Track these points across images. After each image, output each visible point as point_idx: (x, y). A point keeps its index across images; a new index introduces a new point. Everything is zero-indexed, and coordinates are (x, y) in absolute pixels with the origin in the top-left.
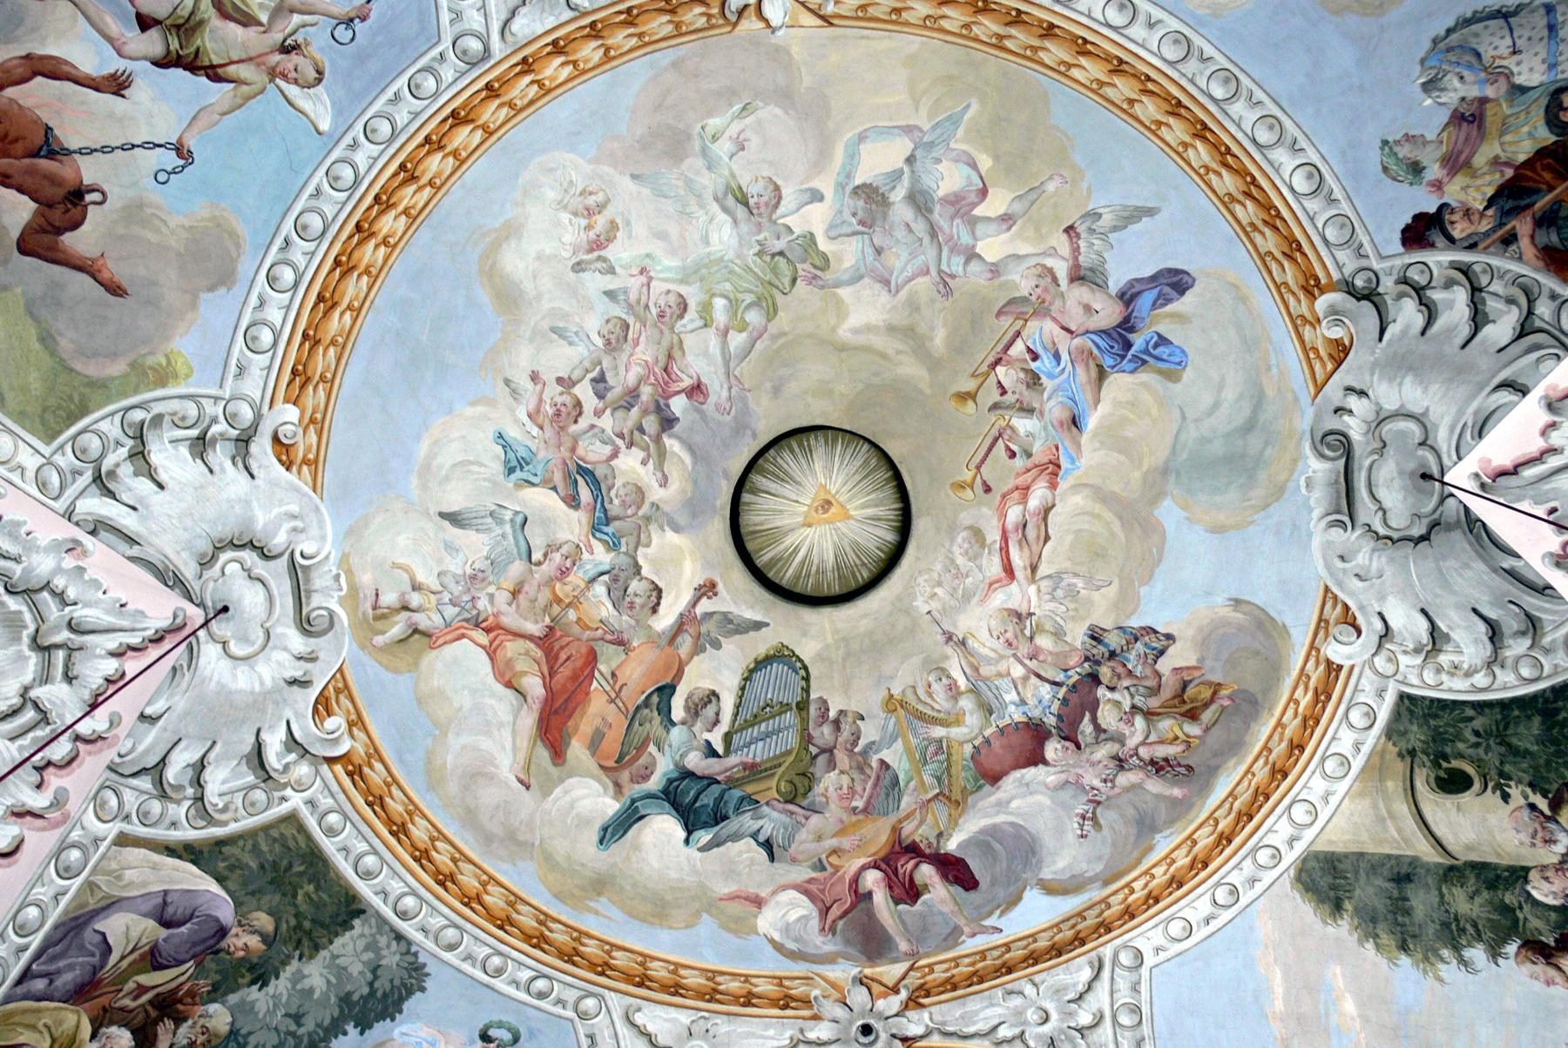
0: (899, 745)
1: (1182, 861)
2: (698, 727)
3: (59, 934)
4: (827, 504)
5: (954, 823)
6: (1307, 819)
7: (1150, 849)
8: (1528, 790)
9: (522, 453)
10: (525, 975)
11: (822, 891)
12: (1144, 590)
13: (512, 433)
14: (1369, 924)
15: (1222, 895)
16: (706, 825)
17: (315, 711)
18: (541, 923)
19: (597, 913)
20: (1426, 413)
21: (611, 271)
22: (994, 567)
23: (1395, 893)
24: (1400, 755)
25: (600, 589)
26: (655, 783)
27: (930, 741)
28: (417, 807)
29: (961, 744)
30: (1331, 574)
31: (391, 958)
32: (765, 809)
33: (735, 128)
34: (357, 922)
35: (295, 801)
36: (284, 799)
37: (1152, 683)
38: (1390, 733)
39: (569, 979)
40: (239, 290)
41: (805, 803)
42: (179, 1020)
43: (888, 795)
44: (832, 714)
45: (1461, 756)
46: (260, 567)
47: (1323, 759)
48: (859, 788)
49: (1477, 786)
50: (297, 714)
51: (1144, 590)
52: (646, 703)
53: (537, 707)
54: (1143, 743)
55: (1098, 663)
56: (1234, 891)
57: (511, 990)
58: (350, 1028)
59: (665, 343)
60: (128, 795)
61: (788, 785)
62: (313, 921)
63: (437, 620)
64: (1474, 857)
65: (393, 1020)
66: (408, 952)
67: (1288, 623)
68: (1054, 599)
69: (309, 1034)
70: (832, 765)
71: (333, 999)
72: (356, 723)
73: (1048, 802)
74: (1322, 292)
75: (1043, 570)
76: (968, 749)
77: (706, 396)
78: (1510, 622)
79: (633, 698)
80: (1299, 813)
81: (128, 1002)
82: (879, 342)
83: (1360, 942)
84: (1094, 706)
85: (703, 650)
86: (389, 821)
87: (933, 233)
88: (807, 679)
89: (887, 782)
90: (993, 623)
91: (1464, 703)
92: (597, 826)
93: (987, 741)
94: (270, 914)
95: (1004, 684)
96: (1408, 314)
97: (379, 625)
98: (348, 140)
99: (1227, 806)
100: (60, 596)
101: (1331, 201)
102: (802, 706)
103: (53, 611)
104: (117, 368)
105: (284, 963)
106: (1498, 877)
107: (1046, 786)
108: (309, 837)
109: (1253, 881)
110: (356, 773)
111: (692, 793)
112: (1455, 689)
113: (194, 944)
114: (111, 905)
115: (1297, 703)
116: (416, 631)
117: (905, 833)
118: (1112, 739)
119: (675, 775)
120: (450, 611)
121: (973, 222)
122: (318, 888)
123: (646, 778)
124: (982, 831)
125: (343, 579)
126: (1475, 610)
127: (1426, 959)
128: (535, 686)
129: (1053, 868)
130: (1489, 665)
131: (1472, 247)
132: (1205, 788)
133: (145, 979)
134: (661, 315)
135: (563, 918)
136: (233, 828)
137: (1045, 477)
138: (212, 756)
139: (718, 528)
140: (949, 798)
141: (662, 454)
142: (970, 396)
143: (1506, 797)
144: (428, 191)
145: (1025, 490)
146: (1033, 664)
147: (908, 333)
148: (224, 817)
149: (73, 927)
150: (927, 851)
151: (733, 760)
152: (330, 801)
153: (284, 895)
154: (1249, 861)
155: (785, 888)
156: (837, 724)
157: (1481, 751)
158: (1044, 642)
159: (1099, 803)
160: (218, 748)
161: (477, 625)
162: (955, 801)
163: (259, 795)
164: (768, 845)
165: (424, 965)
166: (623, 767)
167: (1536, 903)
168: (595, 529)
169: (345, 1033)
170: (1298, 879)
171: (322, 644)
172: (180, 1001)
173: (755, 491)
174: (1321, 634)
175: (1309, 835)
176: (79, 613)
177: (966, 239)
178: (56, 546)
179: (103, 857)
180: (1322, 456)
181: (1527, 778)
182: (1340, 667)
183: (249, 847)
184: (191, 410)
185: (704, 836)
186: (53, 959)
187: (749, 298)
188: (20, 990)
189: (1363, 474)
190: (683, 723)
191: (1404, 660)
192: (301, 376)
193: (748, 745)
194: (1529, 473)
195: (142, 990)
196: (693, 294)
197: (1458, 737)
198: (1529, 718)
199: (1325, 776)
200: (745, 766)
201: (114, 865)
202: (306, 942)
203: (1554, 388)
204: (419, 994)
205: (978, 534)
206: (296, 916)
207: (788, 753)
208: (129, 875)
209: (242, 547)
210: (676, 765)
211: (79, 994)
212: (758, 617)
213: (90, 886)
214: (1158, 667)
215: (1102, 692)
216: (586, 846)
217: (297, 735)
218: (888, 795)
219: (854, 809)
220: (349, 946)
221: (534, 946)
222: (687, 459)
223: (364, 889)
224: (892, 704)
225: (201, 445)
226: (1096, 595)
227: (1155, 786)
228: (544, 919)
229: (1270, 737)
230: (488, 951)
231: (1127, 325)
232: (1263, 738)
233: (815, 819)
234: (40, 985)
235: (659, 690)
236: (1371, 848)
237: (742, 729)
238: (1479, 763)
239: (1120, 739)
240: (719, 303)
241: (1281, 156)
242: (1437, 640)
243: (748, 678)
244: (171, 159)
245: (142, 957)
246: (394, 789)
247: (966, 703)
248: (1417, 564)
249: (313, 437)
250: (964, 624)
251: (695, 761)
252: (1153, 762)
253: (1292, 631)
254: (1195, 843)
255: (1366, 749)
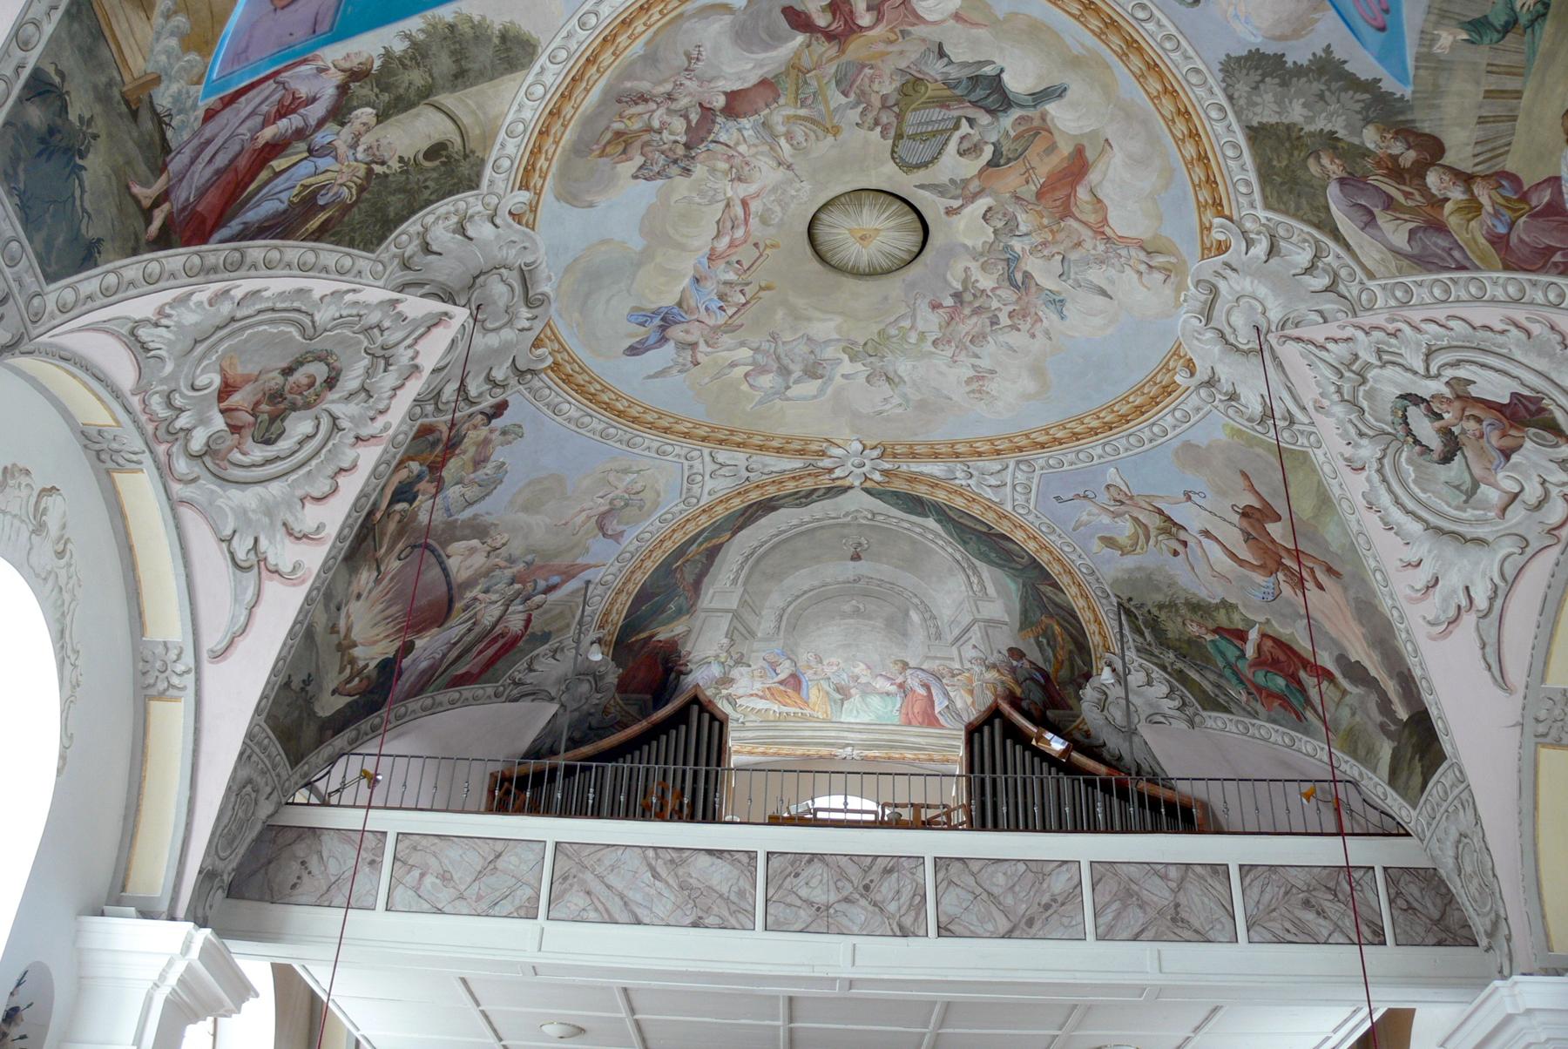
0: (833, 105)
1: (622, 39)
2: (976, 138)
3: (1430, 266)
4: (863, 238)
5: (797, 54)
6: (532, 89)
7: (647, 43)
8: (387, 171)
9: (1052, 307)
10: (1150, 26)
11: (905, 16)
12: (654, 200)
13: (1055, 317)
14: (479, 33)
15: (593, 20)
16: (986, 77)
17: (1227, 249)
18: (1126, 55)
19: (1083, 46)
20: (484, 335)
21: (973, 366)
22: (755, 206)
23: (463, 63)
24: (473, 152)
25: (1023, 229)
26: (1016, 113)
27: (809, 106)
28: (1186, 164)
29: (786, 105)
30: (531, 237)
31: (1242, 89)
32: (939, 78)
33: (888, 407)
34: (1255, 124)
35: (1262, 214)
36: (1268, 220)
37: (647, 149)
38: (482, 162)
39: (1118, 9)
40: (1184, 437)
41: (909, 77)
42: (1395, 158)
43: (845, 75)
44: (879, 129)
45: (434, 169)
46: (1227, 331)
47: (525, 131)
48: (866, 80)
49: (420, 156)
50: (1239, 254)
51: (654, 200)
52: (1009, 160)
53: (1085, 182)
54: (653, 111)
55: (685, 156)
56: (582, 25)
57: (1164, 21)
58: (1290, 64)
59: (951, 328)
60: (1355, 292)
61: (918, 88)
62: (1283, 145)
63: (1133, 252)
64: (413, 111)
65: (1258, 50)
66: (1228, 85)
67: (556, 204)
68: (715, 190)
69: (1319, 81)
70: (884, 98)
71: (1293, 90)
72: (1206, 229)
73: (724, 67)
74: (550, 367)
75: (722, 205)
76: (782, 101)
77: (930, 303)
78: (421, 260)
79: (1018, 167)
80: (539, 90)
81: (1417, 196)
82: (818, 314)
83: (484, 18)
84: (689, 130)
85: (962, 180)
86: (1207, 167)
87: (778, 358)
88: (893, 152)
89: (844, 82)
90: (758, 174)
91: (437, 201)
92: (1064, 100)
93: (767, 106)
94: (1307, 169)
95: (753, 141)
96: (499, 374)
97: (1169, 267)
98: (1102, 460)
99: (591, 83)
100: (1339, 390)
101: (548, 405)
102: (899, 136)
103: (1347, 388)
104: (1259, 450)
105: (1311, 135)
106: (395, 107)
107: (725, 79)
108: (1263, 190)
109: (569, 36)
110: (1217, 204)
111: (991, 99)
112: (444, 207)
113: (1362, 189)
114: (1397, 252)
115: (546, 159)
116: (1149, 253)
117: (836, 48)
118: (676, 111)
119: (1000, 114)
120: (1124, 252)
121: (754, 363)
122: (1270, 160)
123: (1021, 118)
124: (775, 48)
125: (1182, 298)
126: (440, 254)
127: (434, 27)
128: (1082, 193)
129: (722, 23)
130: (426, 230)
131: (470, 416)
132: (606, 92)
133: (1401, 198)
134: (949, 342)
135: (1108, 51)
136: (1306, 229)
137: (717, 254)
138: (1298, 271)
139: (936, 239)
140: (799, 70)
141: (965, 282)
142: (761, 289)
143: (401, 159)
144: (1068, 426)
145: (731, 245)
146: (731, 152)
147: (797, 316)
148: (1308, 237)
149: (1423, 262)
150: (819, 35)
151: (956, 113)
152: (1240, 199)
153: (1293, 171)
154: (572, 50)
155: (934, 23)
156: (876, 123)
157: (422, 178)
158: (723, 166)
159: (686, 70)
160: (1293, 272)
161: (1109, 238)
162: (795, 68)
163: (1281, 232)
164: (942, 54)
165: (1220, 70)
166: (1035, 128)
167: (368, 104)
168: (1018, 259)
169: (1295, 63)
170: (534, 47)
171: (1208, 275)
172: (1387, 168)
173: (909, 251)
174: (534, 203)
175: (530, 79)
176: (1334, 378)
177: (759, 357)
178: (1328, 414)
179: (1385, 278)
180: (542, 294)
181: (391, 178)
182: (520, 189)
183: (1301, 213)
184: (1231, 411)
185: (988, 70)
186: (1443, 259)
187: (894, 340)
188: (1468, 265)
189: (517, 292)
190: (986, 143)
191: (480, 208)
192: (1168, 390)
193: (943, 120)
194: (422, 330)
195: (1407, 195)
196: (927, 346)
197: (437, 180)
198: (397, 214)
199: (523, 121)
200: (948, 107)
201: (1382, 269)
202: (1294, 135)
203: (417, 378)
204: (1233, 55)
205: (764, 221)
206: (1291, 155)
207: (915, 110)
208: (1378, 257)
209: (1232, 344)
210: (998, 120)
211: (1440, 228)
212: (921, 191)
213: (1401, 272)
214: (643, 159)
215: (683, 139)
216: (1076, 90)
217: (1244, 244)
218: (845, 75)
219: (872, 68)
220: (1266, 114)
221: (1136, 42)
222: (949, 277)
223: (1241, 139)
224: (836, 131)
225: (1233, 397)
226: (686, 194)
227: (644, 86)
228: (1123, 56)
229: (563, 133)
230: (1172, 55)
231: (663, 328)
232: (568, 132)
233: (903, 65)
234: (1456, 254)
235: (998, 165)
236: (485, 86)
237: (945, 130)
238: (422, 170)
239: (670, 112)
240: (913, 340)
241: (574, 413)
242: (461, 230)
243: (934, 159)
244: (1194, 497)
245: (1395, 210)
246: (1197, 182)
247: (781, 129)
248: (481, 261)
249: (1171, 364)
250: (781, 174)
251: (984, 119)
252: (646, 101)
253: (553, 199)
254: (614, 53)
255: (497, 146)
